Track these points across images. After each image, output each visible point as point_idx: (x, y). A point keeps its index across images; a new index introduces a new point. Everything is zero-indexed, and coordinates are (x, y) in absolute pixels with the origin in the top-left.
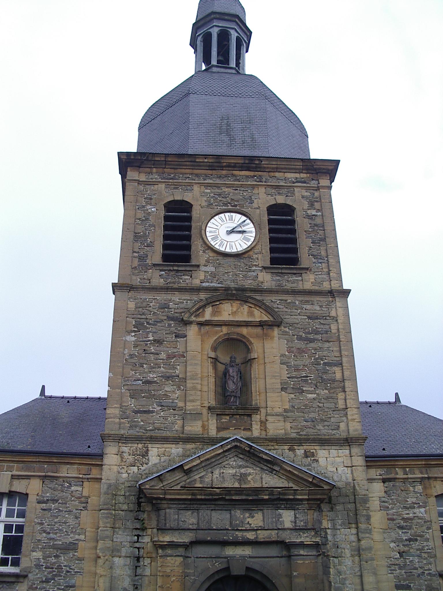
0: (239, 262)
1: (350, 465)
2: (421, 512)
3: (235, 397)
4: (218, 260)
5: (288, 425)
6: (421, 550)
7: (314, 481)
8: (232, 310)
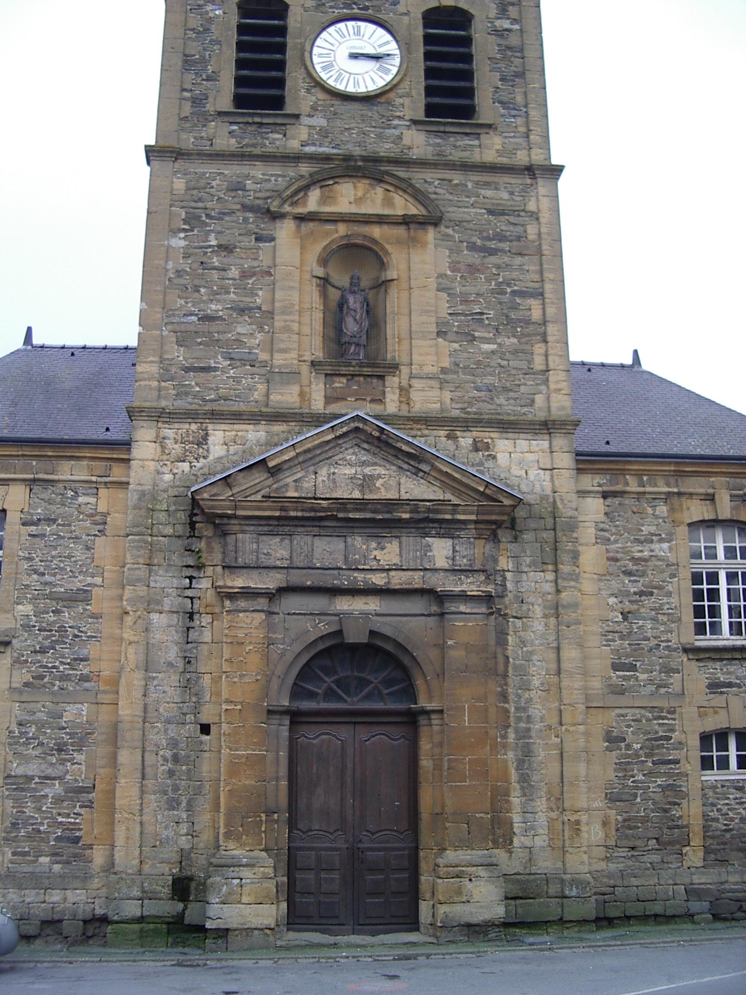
0: (371, 110)
1: (549, 467)
2: (662, 549)
3: (358, 345)
4: (332, 106)
5: (447, 396)
6: (658, 610)
7: (488, 491)
8: (355, 194)
